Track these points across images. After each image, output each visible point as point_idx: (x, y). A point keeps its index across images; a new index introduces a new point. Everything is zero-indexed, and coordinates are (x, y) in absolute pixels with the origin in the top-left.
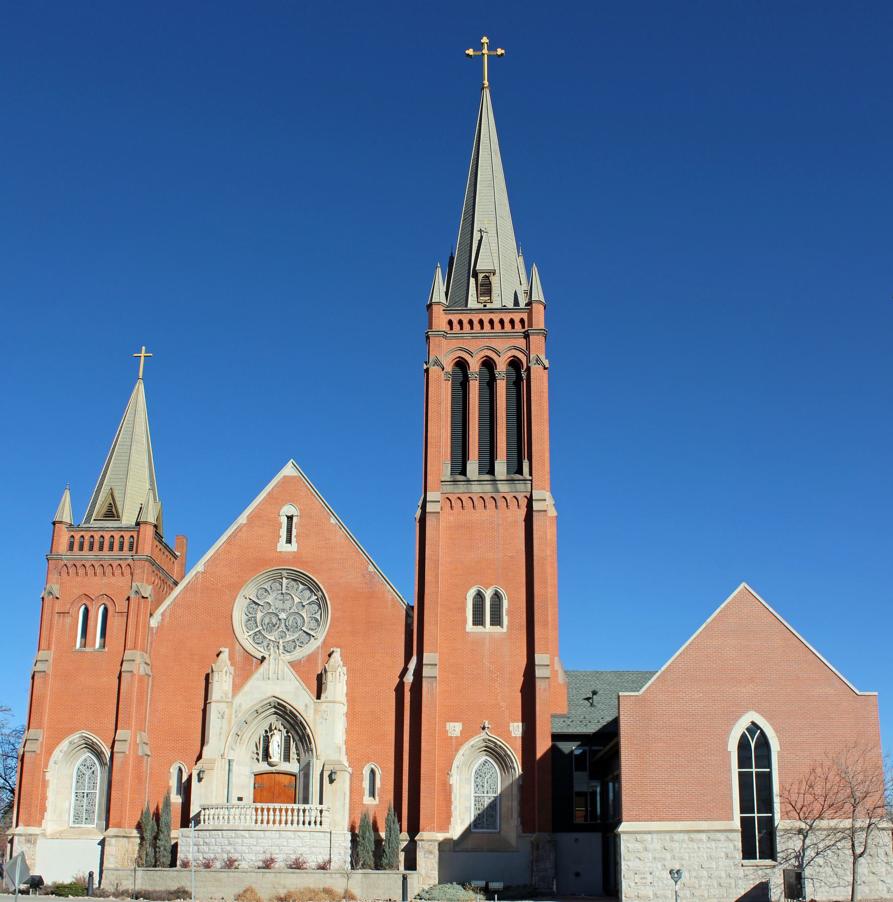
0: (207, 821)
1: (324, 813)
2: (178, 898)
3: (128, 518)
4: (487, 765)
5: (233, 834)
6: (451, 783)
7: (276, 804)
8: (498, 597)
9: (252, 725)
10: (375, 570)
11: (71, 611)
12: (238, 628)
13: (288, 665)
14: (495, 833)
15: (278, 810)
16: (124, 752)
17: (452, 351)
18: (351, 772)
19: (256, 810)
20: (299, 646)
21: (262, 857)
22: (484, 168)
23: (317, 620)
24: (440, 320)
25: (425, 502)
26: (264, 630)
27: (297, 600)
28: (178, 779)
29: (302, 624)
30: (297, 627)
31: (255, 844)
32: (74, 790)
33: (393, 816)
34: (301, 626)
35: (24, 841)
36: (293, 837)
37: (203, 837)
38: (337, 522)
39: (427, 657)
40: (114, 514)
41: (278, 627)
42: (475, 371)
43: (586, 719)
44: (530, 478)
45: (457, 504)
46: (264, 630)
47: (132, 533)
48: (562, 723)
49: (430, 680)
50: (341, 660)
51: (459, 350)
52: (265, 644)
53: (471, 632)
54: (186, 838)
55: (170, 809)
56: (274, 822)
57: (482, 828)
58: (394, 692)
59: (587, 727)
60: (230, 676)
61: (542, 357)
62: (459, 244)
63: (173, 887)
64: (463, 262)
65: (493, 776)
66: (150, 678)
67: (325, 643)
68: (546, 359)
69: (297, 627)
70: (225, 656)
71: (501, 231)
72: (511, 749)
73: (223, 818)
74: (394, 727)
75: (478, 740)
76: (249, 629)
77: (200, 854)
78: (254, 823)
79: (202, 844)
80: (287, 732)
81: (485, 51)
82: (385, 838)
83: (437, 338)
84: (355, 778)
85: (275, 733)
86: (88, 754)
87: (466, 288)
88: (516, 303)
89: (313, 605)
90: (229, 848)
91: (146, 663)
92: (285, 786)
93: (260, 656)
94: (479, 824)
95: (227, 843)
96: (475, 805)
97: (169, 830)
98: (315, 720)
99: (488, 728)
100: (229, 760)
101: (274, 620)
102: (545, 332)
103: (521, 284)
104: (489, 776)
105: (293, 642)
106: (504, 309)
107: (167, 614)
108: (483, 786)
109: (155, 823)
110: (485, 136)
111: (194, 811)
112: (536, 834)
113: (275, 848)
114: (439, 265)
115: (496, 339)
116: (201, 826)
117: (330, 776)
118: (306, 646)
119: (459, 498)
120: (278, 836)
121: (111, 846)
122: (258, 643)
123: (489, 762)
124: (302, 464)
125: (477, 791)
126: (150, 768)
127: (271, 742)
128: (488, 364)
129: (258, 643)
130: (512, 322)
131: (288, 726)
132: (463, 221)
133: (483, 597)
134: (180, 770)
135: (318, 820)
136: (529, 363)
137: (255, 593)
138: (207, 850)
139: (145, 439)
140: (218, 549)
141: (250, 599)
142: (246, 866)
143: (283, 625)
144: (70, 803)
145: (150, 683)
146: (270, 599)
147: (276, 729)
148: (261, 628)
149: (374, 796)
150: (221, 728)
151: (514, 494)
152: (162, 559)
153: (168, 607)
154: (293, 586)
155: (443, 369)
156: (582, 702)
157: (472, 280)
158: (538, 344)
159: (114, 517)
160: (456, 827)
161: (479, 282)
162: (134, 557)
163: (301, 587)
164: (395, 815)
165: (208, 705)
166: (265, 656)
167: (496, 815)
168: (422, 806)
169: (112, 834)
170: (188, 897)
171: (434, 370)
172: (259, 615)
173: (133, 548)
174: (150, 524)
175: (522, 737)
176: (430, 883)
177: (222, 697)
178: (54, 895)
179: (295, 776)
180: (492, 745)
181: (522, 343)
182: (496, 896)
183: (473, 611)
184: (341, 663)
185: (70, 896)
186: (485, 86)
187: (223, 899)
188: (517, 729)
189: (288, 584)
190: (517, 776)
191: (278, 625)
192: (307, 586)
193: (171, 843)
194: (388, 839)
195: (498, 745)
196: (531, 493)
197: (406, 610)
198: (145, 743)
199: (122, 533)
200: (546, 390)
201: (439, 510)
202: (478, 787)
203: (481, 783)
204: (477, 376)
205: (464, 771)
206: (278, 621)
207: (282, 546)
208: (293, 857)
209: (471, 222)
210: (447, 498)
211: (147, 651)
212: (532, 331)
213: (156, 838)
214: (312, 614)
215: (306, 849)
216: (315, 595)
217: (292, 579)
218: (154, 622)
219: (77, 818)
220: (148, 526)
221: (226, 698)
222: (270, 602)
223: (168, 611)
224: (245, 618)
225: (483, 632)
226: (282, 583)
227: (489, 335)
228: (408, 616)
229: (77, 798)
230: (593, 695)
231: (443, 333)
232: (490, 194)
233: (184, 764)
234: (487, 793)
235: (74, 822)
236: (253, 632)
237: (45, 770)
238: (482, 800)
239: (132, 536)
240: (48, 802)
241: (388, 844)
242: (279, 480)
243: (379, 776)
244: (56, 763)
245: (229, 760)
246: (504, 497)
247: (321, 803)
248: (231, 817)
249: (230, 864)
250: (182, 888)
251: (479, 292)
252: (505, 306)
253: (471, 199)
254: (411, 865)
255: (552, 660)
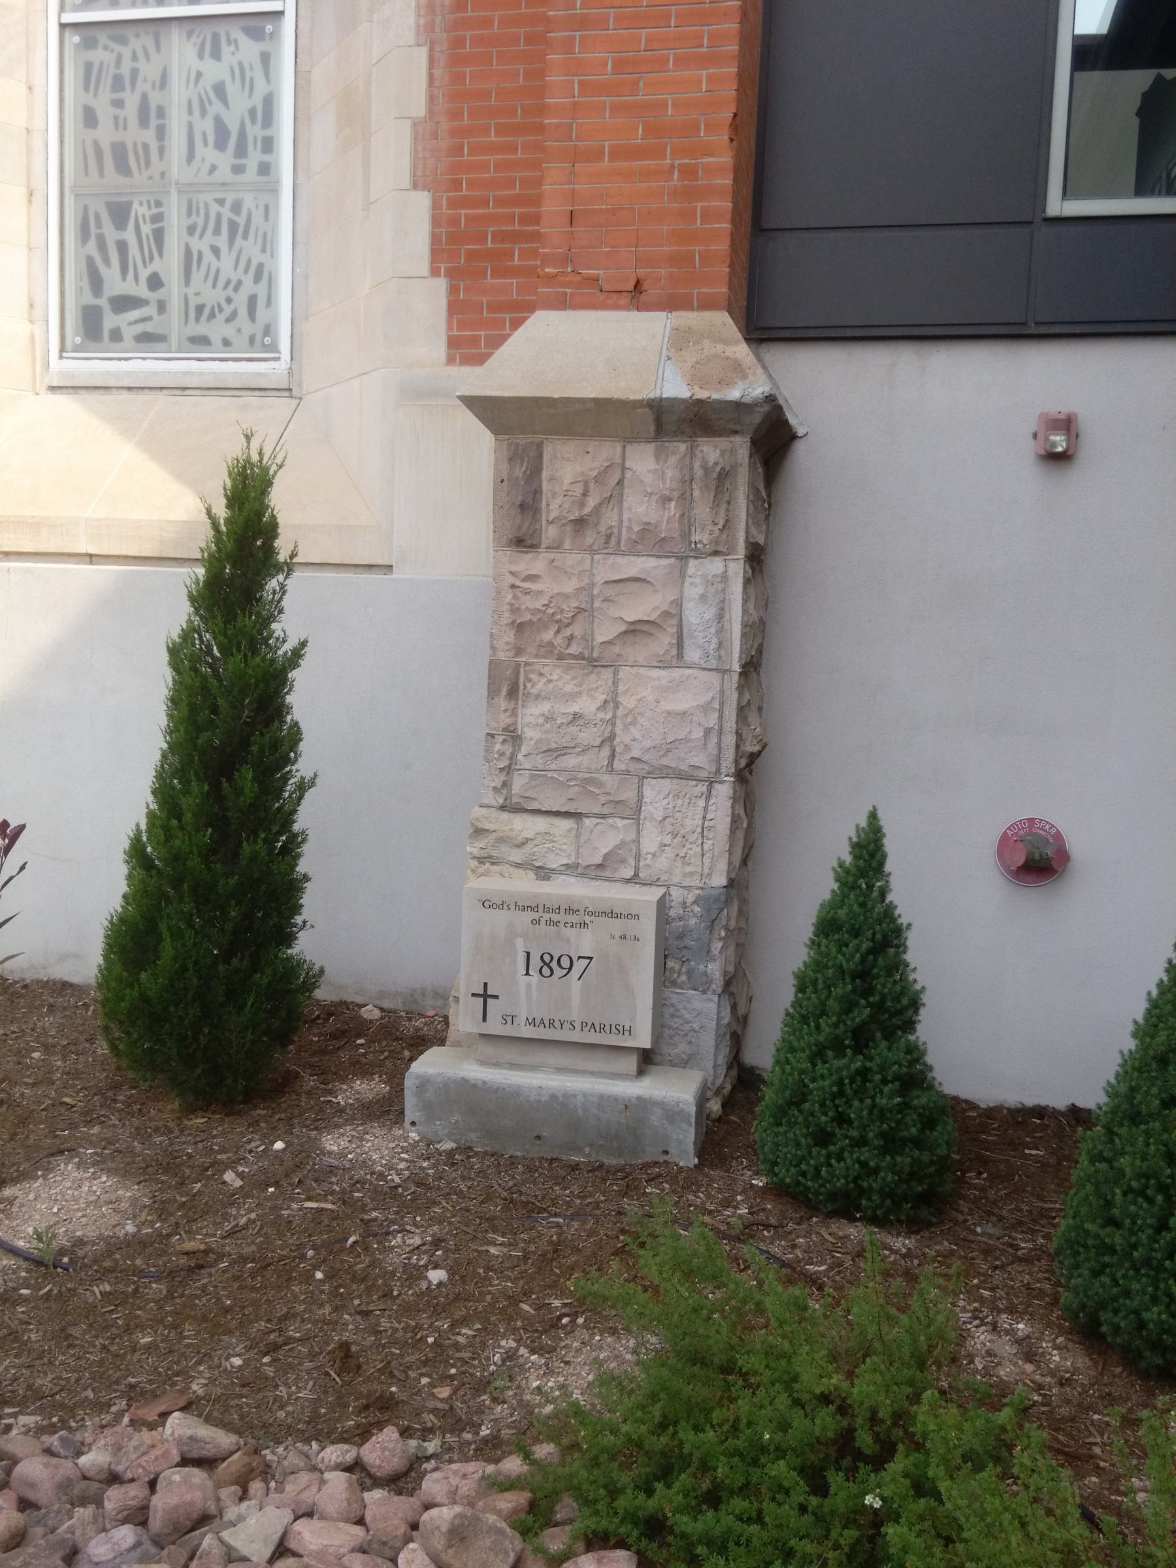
94: (123, 303)
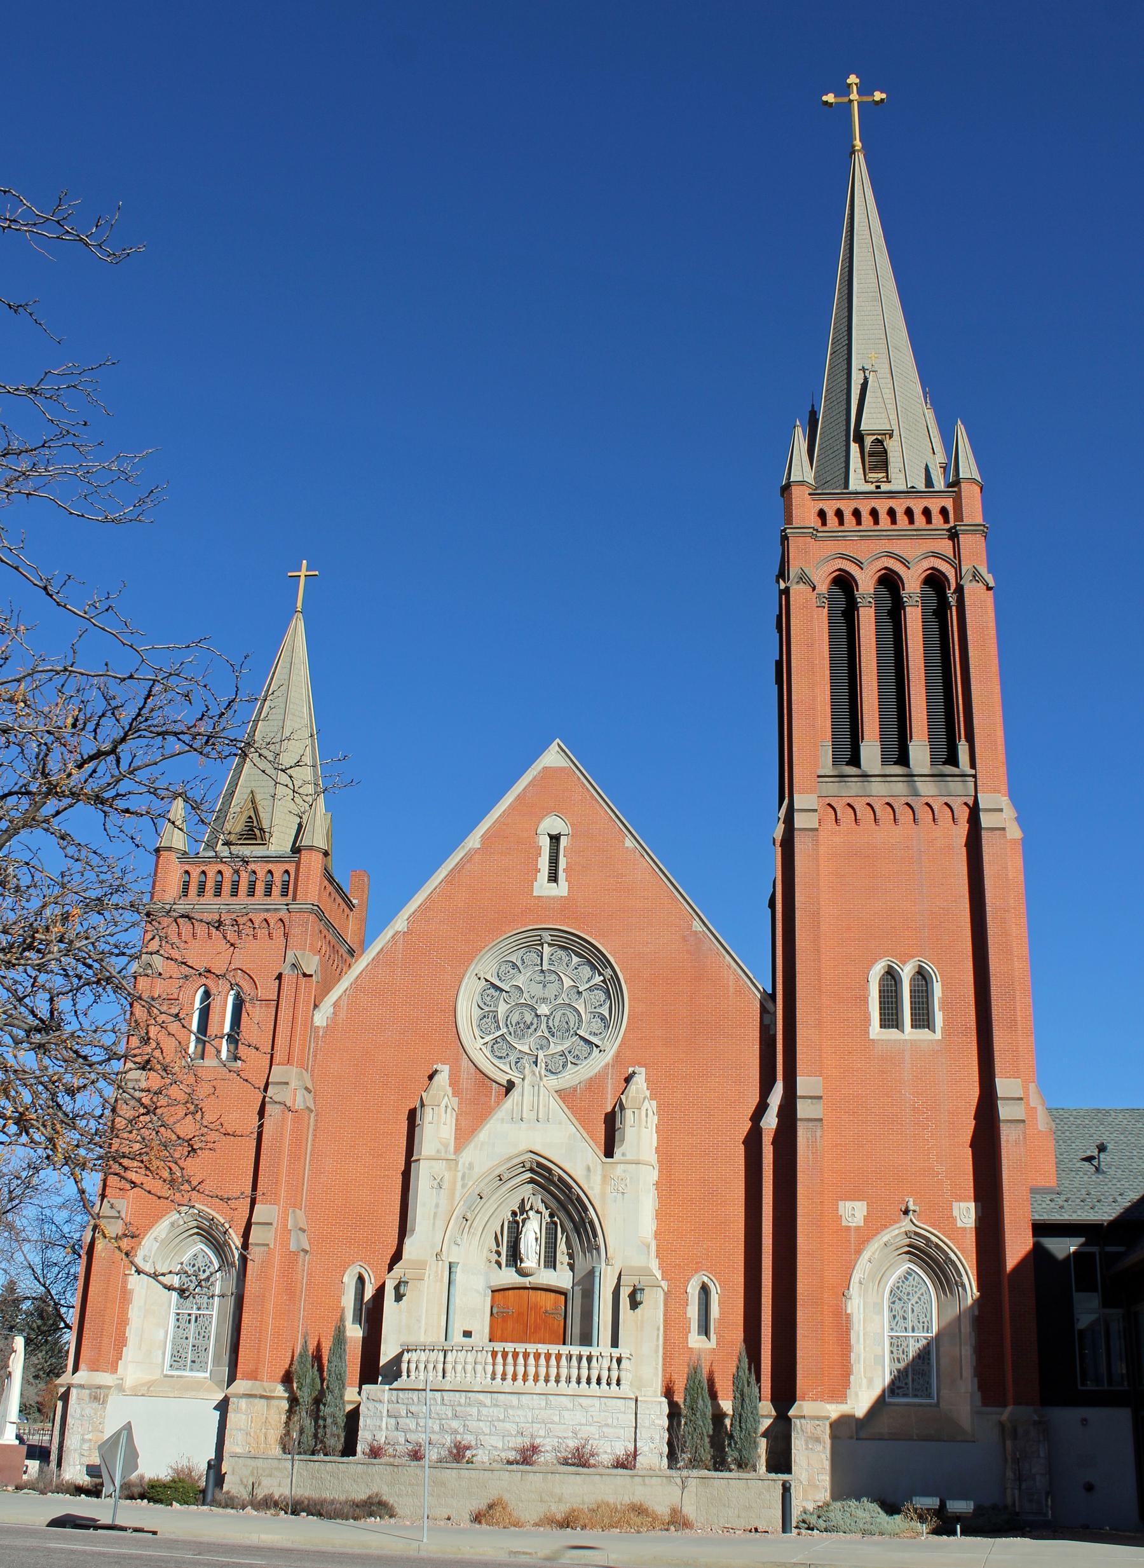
0: (413, 1374)
1: (624, 1362)
2: (371, 1515)
3: (280, 842)
4: (911, 1278)
5: (462, 1398)
6: (849, 1311)
7: (540, 1345)
8: (924, 978)
9: (491, 1201)
10: (705, 929)
11: (181, 996)
12: (466, 1030)
13: (555, 1095)
14: (930, 1405)
15: (542, 1357)
16: (268, 1245)
17: (828, 560)
18: (666, 1289)
19: (494, 1354)
20: (572, 1063)
21: (519, 1442)
22: (863, 272)
23: (603, 1018)
24: (805, 510)
25: (791, 810)
26: (510, 1034)
27: (567, 983)
28: (355, 1299)
29: (577, 1024)
30: (568, 1030)
31: (502, 1417)
32: (173, 1310)
33: (747, 1371)
34: (575, 1029)
35: (87, 1399)
36: (570, 1406)
37: (406, 1401)
38: (637, 845)
39: (804, 1085)
40: (255, 835)
41: (535, 1030)
42: (867, 592)
43: (1091, 1196)
44: (973, 772)
45: (846, 816)
46: (510, 1034)
47: (287, 866)
48: (1049, 1202)
49: (811, 1124)
50: (648, 1089)
51: (840, 557)
52: (513, 1058)
53: (879, 1040)
54: (375, 1403)
55: (344, 1350)
56: (568, 1380)
57: (905, 1395)
58: (742, 1147)
59: (1096, 1210)
60: (452, 1112)
61: (983, 570)
62: (827, 391)
63: (361, 1495)
64: (835, 418)
65: (922, 1299)
66: (312, 1115)
67: (617, 1056)
68: (989, 573)
69: (568, 1030)
70: (442, 1079)
71: (898, 370)
72: (956, 1250)
73: (425, 1367)
74: (742, 1209)
75: (896, 1233)
76: (484, 1032)
77: (400, 1433)
78: (489, 1379)
79: (404, 1415)
80: (551, 1215)
81: (854, 96)
82: (730, 1412)
83: (800, 538)
84: (674, 1300)
85: (531, 1216)
86: (200, 1246)
87: (843, 459)
88: (929, 482)
89: (596, 991)
90: (455, 1424)
91: (307, 1089)
92: (546, 1312)
93: (504, 1079)
94: (899, 1388)
95: (450, 1415)
96: (892, 1352)
97: (342, 1388)
98: (603, 1195)
99: (914, 1211)
100: (450, 1263)
101: (529, 1017)
102: (985, 530)
103: (934, 453)
104: (915, 1299)
105: (561, 1055)
106: (911, 492)
107: (344, 1003)
108: (905, 1318)
109: (316, 1373)
110: (861, 224)
111: (387, 1353)
112: (1009, 1409)
113: (539, 1426)
114: (798, 423)
115: (902, 541)
116: (402, 1382)
117: (632, 1296)
118: (585, 1063)
119: (849, 805)
120: (543, 1404)
121: (238, 1413)
122: (501, 1058)
123: (914, 1274)
124: (575, 747)
125: (894, 1326)
126: (308, 1274)
127: (523, 1233)
128: (890, 582)
129: (501, 1058)
130: (927, 512)
131: (554, 1204)
132: (831, 355)
133: (897, 978)
134: (361, 1279)
135: (615, 1375)
136: (961, 579)
137: (494, 970)
138: (413, 1426)
139: (305, 710)
140: (431, 893)
141: (487, 981)
142: (486, 1459)
143: (544, 1026)
144: (167, 1332)
145: (312, 1124)
146: (520, 981)
147: (531, 1208)
148: (506, 1030)
149: (707, 1334)
150: (437, 1206)
151: (946, 799)
152: (333, 909)
153: (345, 991)
154: (561, 959)
155: (814, 589)
156: (1079, 1165)
157: (854, 448)
158: (973, 548)
159: (256, 839)
160: (860, 1393)
161: (867, 449)
162: (290, 906)
163: (575, 959)
164: (750, 1369)
165: (412, 1164)
166: (514, 1079)
167: (930, 1371)
168: (799, 1354)
169: (241, 1391)
170: (387, 1514)
171: (798, 591)
172: (502, 1009)
173: (287, 892)
174: (317, 849)
175: (976, 1228)
176: (817, 1498)
177: (438, 1151)
178: (146, 1501)
179: (565, 1294)
180: (921, 1243)
181: (946, 547)
182: (958, 1526)
183: (880, 1003)
184: (648, 1093)
185: (174, 1503)
186: (856, 148)
187: (449, 1519)
188: (966, 1214)
189: (553, 954)
190: (970, 1301)
191: (535, 1026)
192: (585, 957)
193: (344, 1410)
194: (739, 1416)
195: (932, 1242)
196: (976, 797)
197: (760, 1001)
198: (301, 1229)
199: (270, 866)
200: (992, 624)
201: (817, 827)
202: (896, 1320)
203: (901, 1313)
204: (871, 600)
205: (870, 1290)
206: (536, 1019)
207: (543, 887)
208: (572, 1444)
209: (846, 356)
210: (829, 805)
211: (308, 1067)
212: (963, 528)
213: (318, 1401)
214: (595, 1008)
215: (593, 1429)
216: (600, 974)
217: (560, 947)
218: (320, 1018)
219: (177, 1359)
220: (314, 853)
221: (446, 1152)
222: (521, 986)
223: (345, 998)
224: (477, 1013)
225: (900, 1040)
226: (542, 953)
227: (889, 533)
228: (766, 1011)
229: (178, 1324)
230: (1099, 1152)
231: (811, 530)
232: (875, 313)
233: (367, 1268)
234: (913, 1331)
235: (171, 1366)
236: (491, 1037)
237: (126, 1272)
238: (904, 1344)
239: (287, 872)
240: (130, 1330)
241: (738, 1423)
242: (535, 773)
243: (717, 1296)
244: (147, 1259)
245: (450, 1263)
246: (927, 804)
247: (615, 1343)
248: (449, 1367)
249: (459, 1454)
250: (377, 1495)
251: (867, 466)
252: (913, 487)
253: (844, 320)
254: (780, 1462)
255: (1026, 1089)
